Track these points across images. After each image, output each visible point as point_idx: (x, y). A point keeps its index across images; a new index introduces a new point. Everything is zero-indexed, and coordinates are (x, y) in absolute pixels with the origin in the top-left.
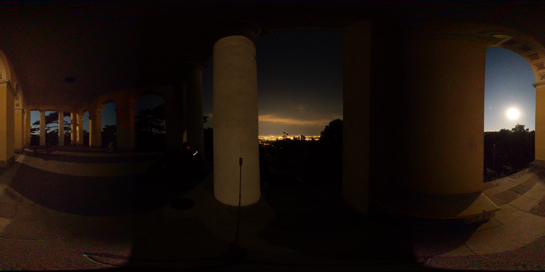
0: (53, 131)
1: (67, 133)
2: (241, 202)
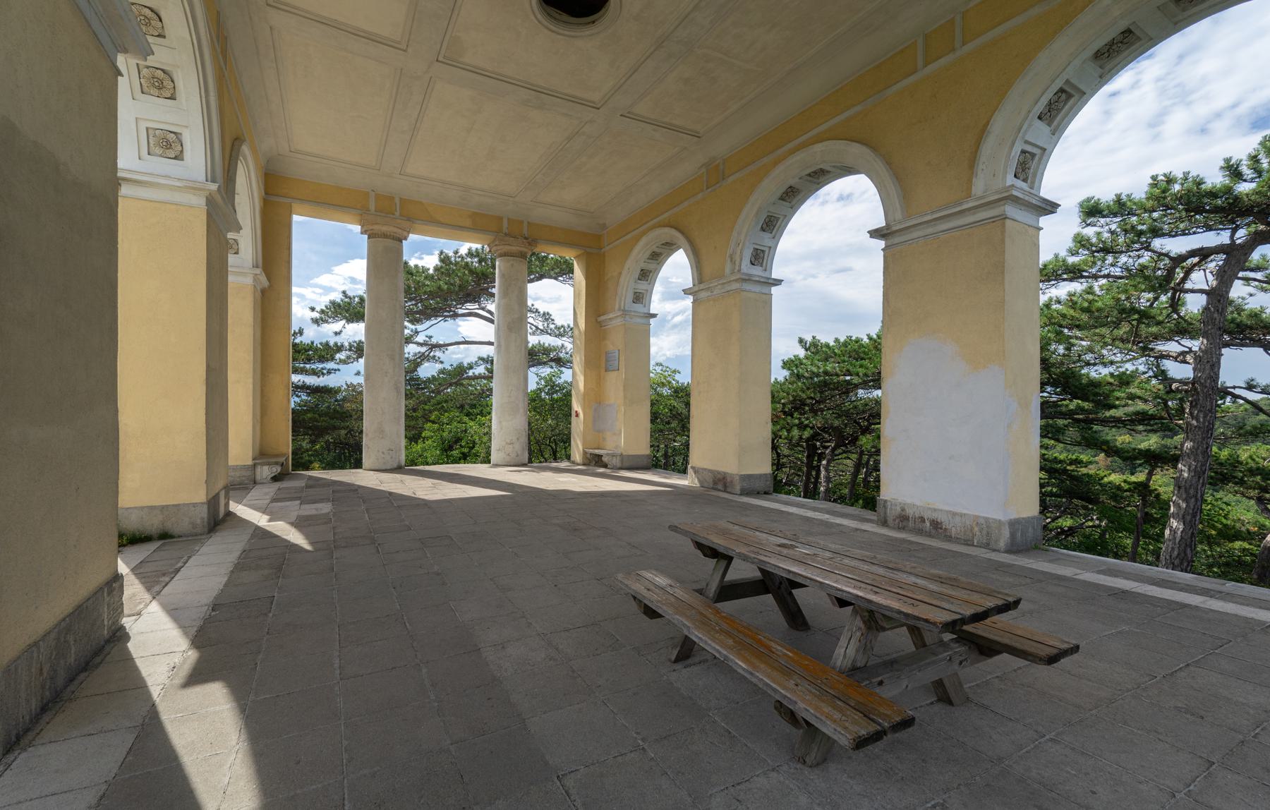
0: (460, 370)
1: (551, 385)
2: (486, 340)
